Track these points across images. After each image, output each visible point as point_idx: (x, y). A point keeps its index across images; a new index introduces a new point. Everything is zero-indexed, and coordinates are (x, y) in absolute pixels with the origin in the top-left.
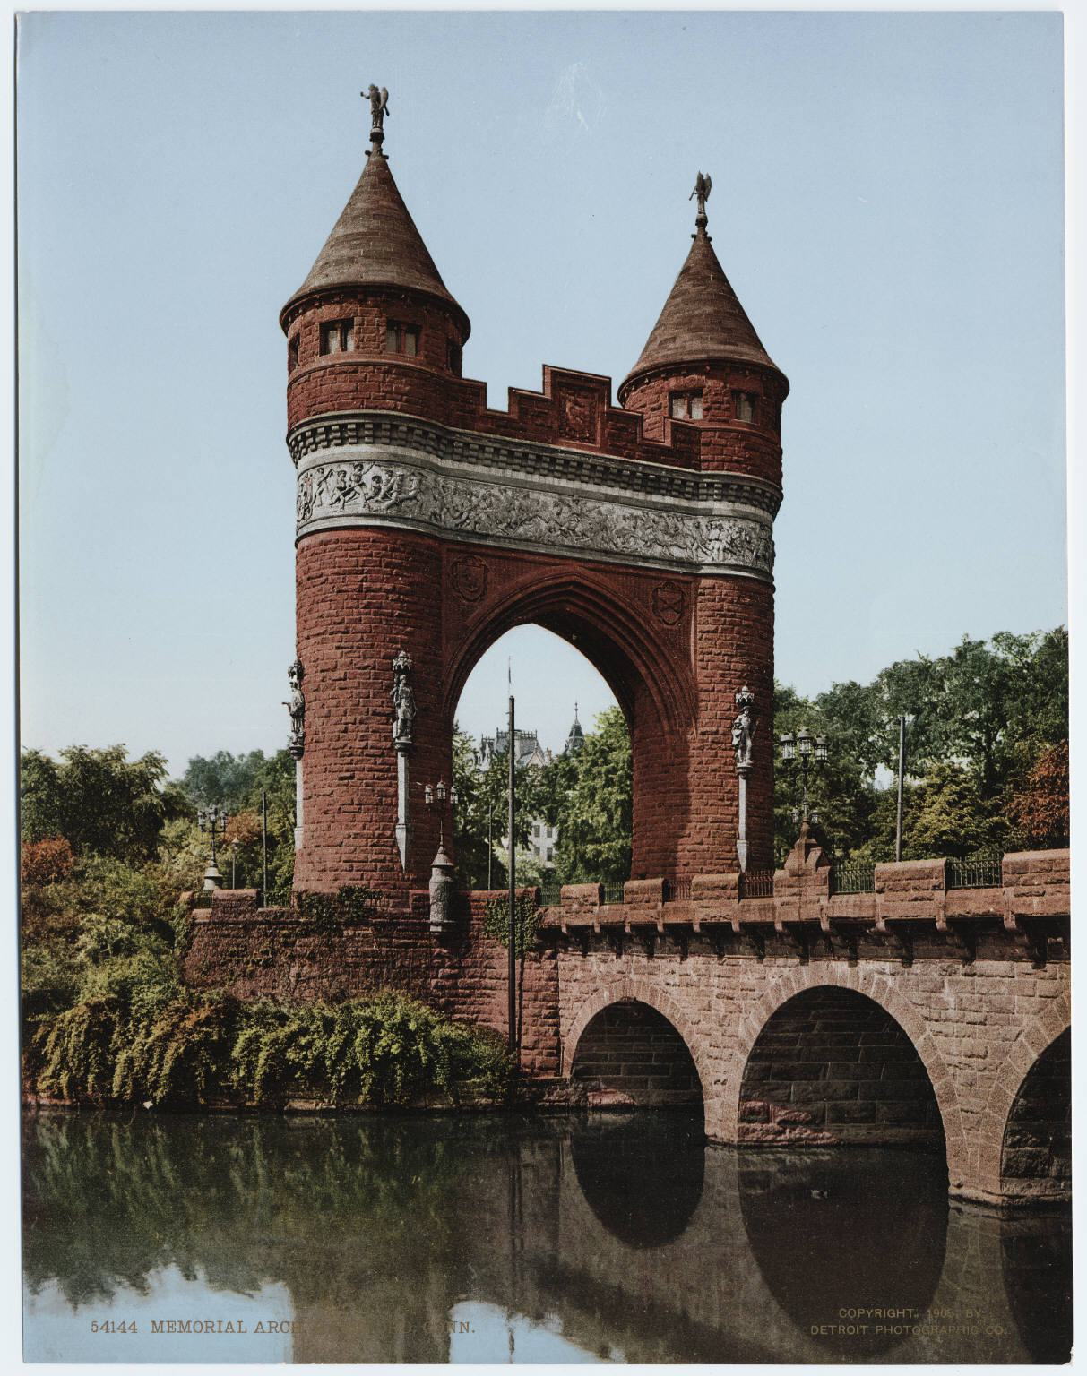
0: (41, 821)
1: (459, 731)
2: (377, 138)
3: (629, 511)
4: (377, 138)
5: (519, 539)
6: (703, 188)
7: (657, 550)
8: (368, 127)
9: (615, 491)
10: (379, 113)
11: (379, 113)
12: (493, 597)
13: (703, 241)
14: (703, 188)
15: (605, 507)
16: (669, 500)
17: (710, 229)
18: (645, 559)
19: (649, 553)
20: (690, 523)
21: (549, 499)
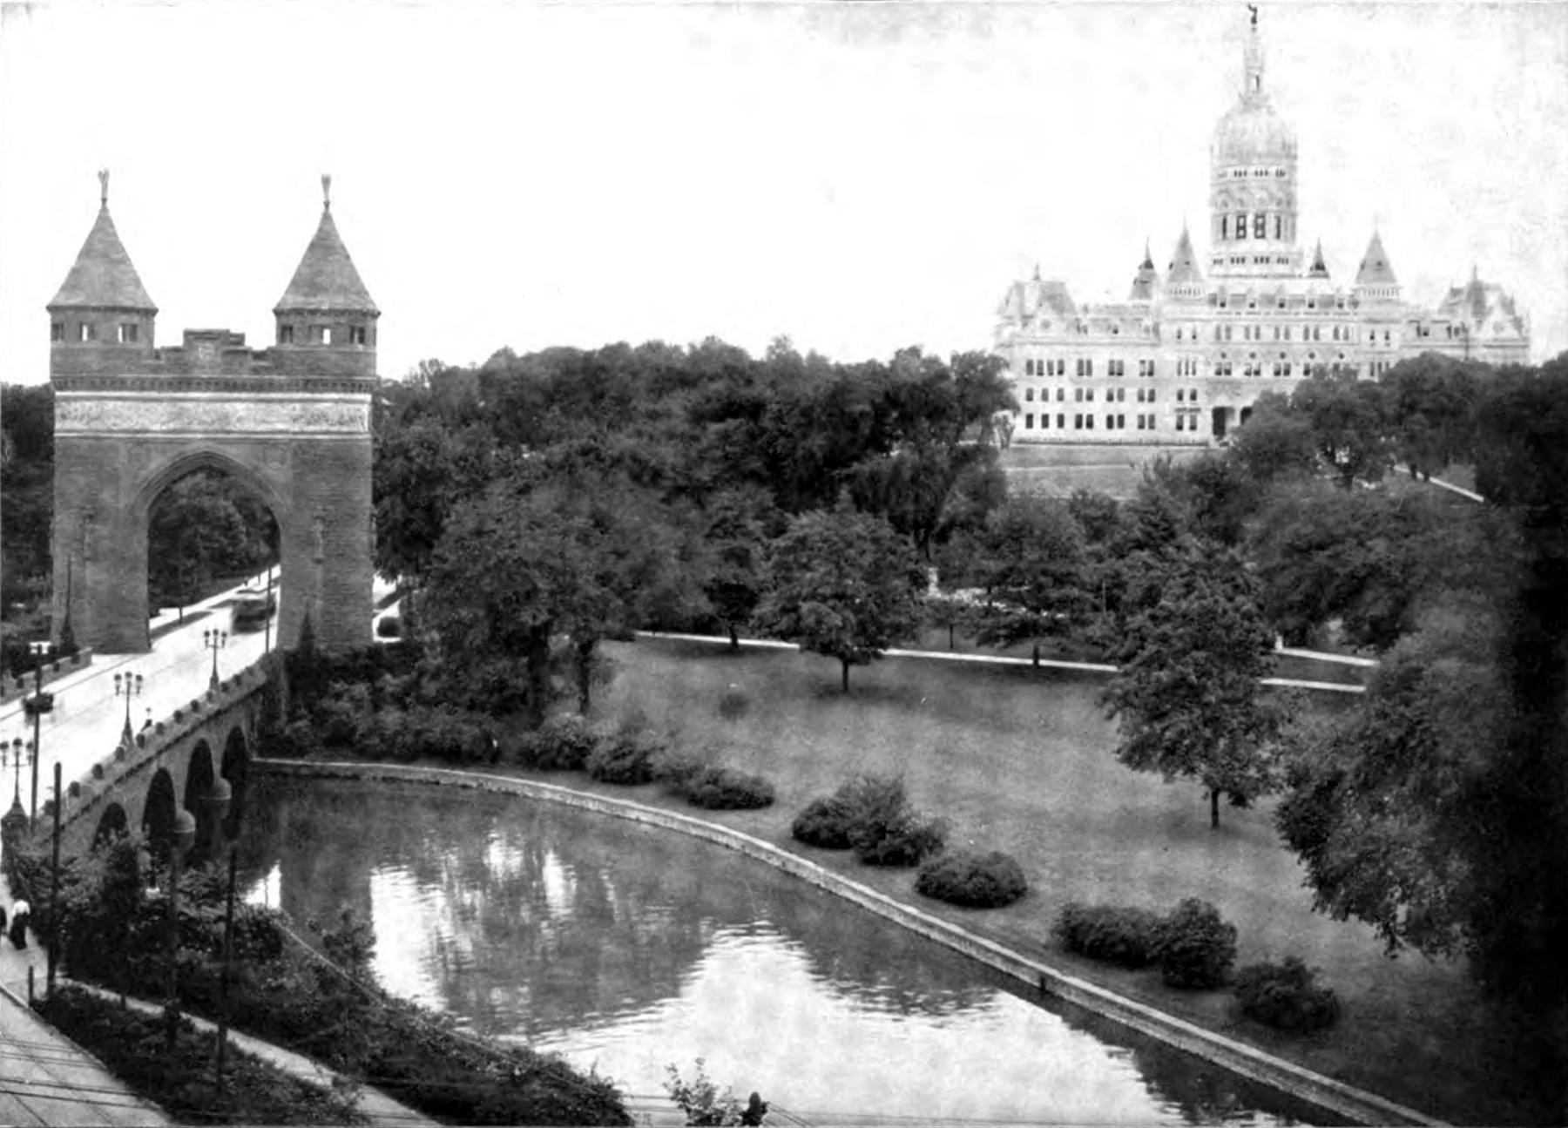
6: (326, 182)
13: (327, 217)
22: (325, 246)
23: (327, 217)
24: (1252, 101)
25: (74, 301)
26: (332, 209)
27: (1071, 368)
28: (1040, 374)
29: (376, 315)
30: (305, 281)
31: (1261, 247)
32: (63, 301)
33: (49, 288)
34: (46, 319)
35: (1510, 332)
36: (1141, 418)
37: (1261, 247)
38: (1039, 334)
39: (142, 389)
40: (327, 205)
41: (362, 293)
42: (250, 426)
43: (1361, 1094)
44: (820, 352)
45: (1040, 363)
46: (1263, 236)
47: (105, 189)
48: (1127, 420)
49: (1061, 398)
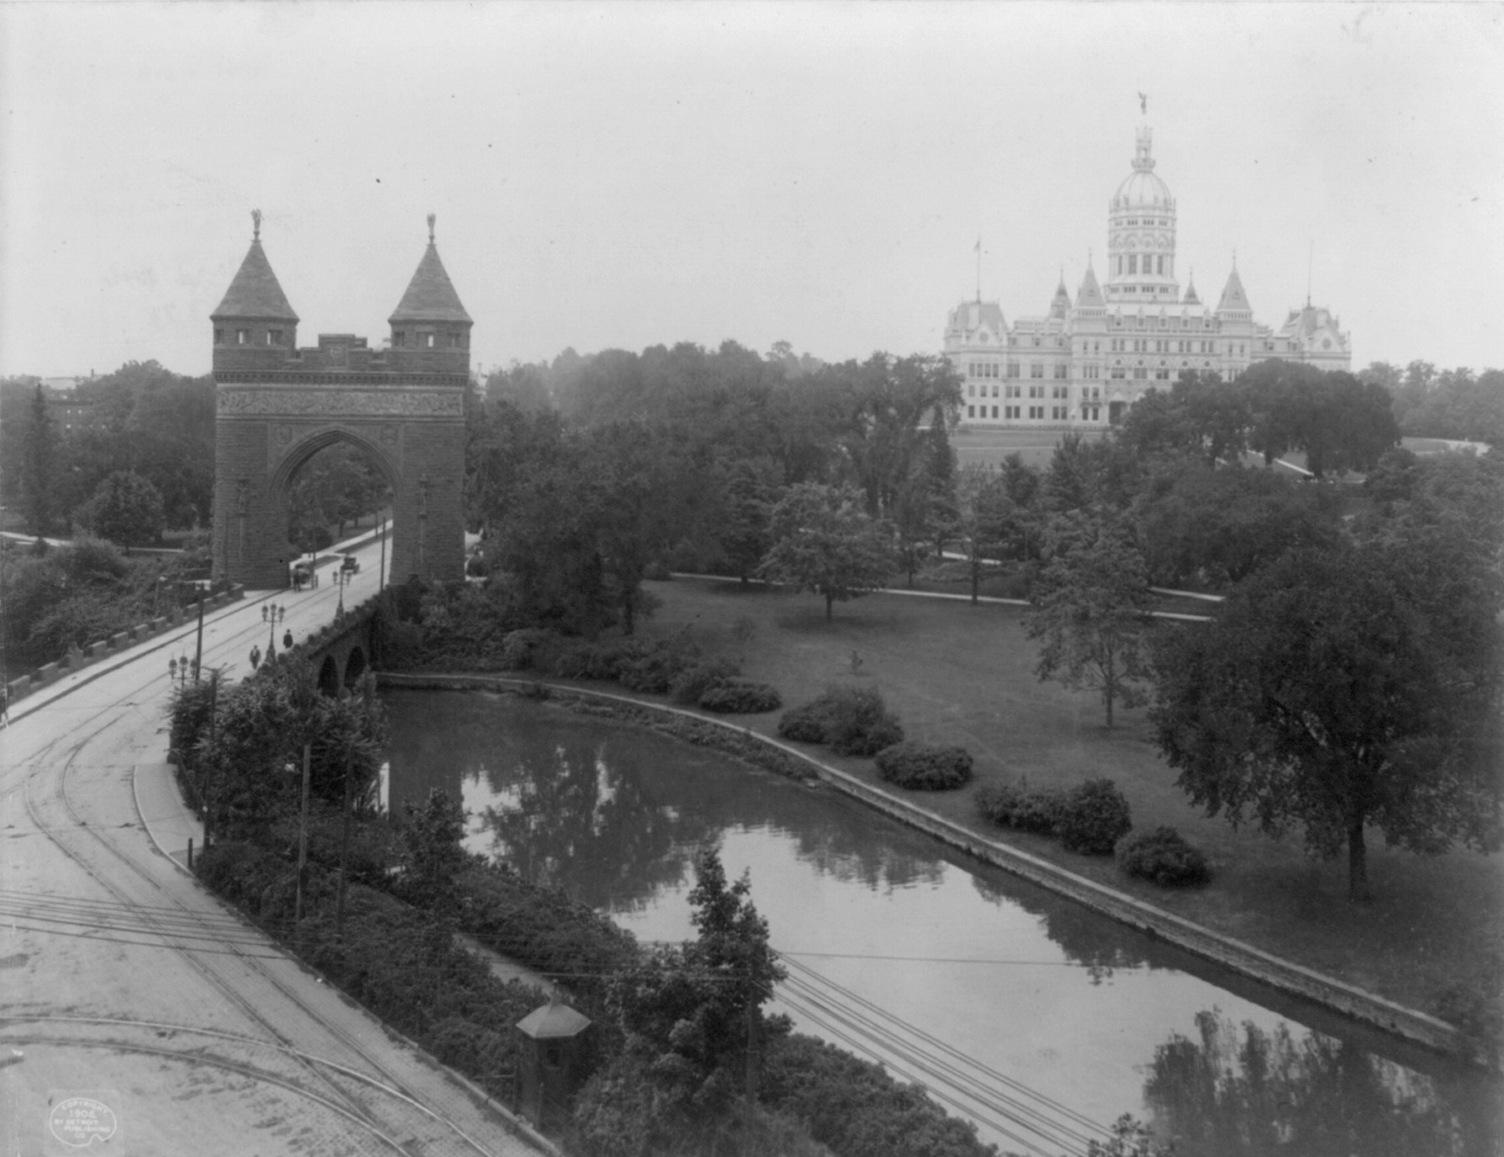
0: (310, 822)
1: (1263, 832)
2: (257, 233)
3: (367, 394)
4: (257, 233)
5: (306, 415)
6: (431, 220)
7: (381, 412)
8: (261, 228)
9: (359, 386)
10: (257, 223)
11: (257, 223)
12: (295, 441)
13: (432, 247)
14: (431, 220)
15: (352, 394)
16: (388, 387)
17: (435, 241)
18: (375, 416)
19: (377, 413)
20: (401, 396)
21: (324, 394)
22: (256, 263)
23: (432, 247)
27: (1003, 371)
37: (1147, 280)
49: (995, 395)
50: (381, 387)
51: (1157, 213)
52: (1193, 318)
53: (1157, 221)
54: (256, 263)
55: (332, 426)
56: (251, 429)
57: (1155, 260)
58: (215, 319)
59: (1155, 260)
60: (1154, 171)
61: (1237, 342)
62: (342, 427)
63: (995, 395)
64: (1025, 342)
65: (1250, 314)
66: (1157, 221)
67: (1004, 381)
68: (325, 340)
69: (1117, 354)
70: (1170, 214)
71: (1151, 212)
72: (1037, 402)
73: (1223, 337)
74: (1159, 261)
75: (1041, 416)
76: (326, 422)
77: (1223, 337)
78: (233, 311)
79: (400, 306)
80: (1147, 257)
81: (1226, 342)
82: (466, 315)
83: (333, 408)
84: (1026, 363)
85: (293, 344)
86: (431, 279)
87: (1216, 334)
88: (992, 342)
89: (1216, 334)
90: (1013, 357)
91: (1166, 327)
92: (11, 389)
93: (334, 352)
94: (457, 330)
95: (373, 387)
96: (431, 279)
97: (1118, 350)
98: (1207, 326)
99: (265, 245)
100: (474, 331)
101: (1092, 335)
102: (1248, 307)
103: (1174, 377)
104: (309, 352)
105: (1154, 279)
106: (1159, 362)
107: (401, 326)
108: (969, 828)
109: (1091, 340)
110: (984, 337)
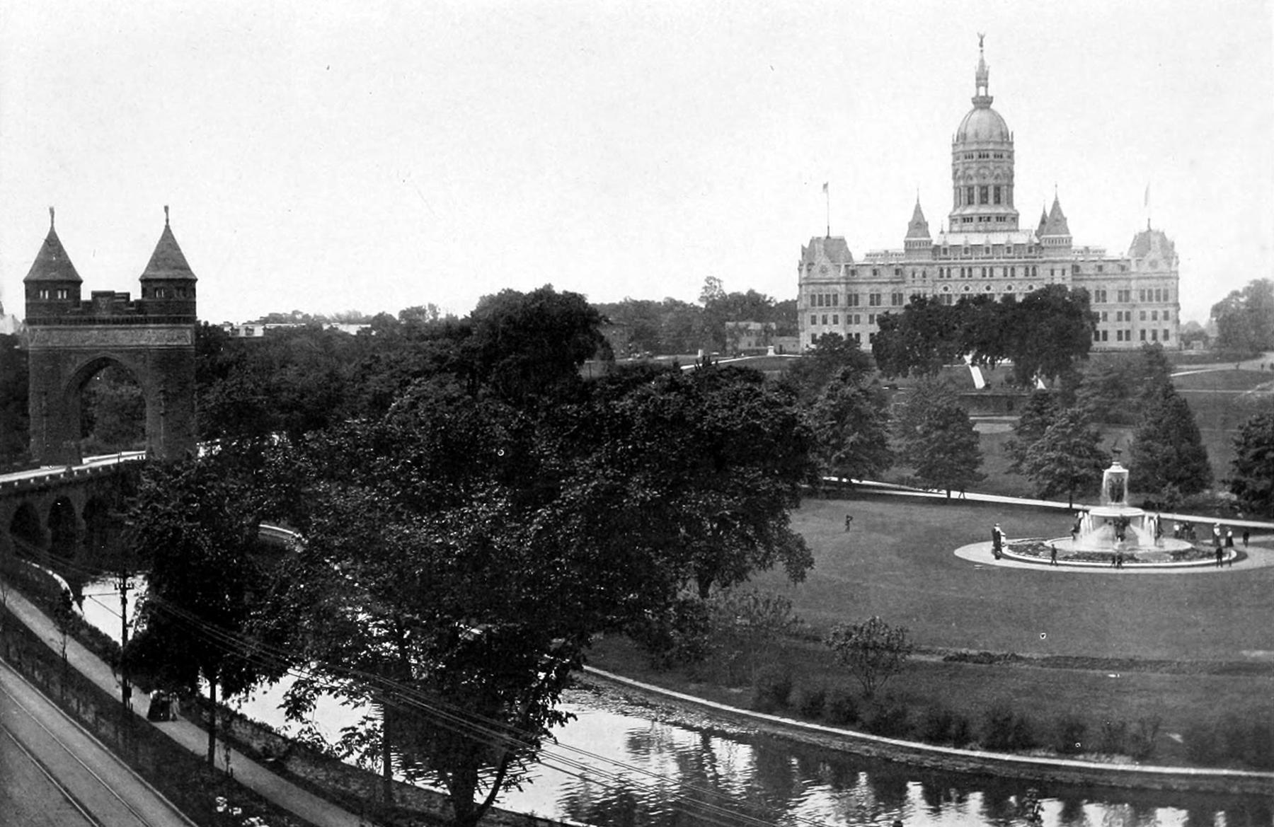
6: (166, 209)
13: (167, 227)
14: (166, 209)
22: (52, 243)
23: (167, 227)
24: (983, 103)
25: (162, 274)
26: (170, 223)
27: (842, 300)
28: (821, 304)
29: (196, 280)
30: (41, 263)
31: (984, 210)
32: (152, 275)
33: (25, 269)
34: (23, 286)
35: (1163, 267)
36: (1120, 332)
37: (984, 210)
38: (1150, 270)
39: (159, 323)
40: (167, 221)
41: (187, 268)
42: (125, 343)
43: (183, 815)
44: (759, 291)
45: (1158, 291)
46: (986, 202)
47: (53, 217)
48: (1110, 334)
49: (1155, 318)
50: (133, 326)
51: (991, 146)
52: (1016, 245)
53: (991, 154)
54: (52, 243)
55: (99, 355)
56: (55, 357)
57: (991, 192)
58: (27, 282)
59: (991, 192)
60: (992, 106)
61: (920, 269)
62: (108, 354)
63: (836, 322)
64: (887, 275)
65: (1070, 239)
66: (991, 154)
67: (845, 310)
68: (96, 295)
69: (1008, 280)
70: (1005, 147)
71: (984, 147)
72: (1124, 326)
73: (1044, 262)
74: (1000, 191)
75: (1128, 338)
76: (97, 351)
77: (1044, 262)
78: (36, 277)
79: (147, 268)
80: (984, 188)
81: (1049, 266)
82: (192, 274)
83: (103, 341)
84: (865, 291)
85: (79, 297)
86: (168, 249)
87: (1038, 259)
88: (831, 274)
89: (1038, 259)
90: (853, 287)
91: (1011, 255)
92: (1, 335)
93: (102, 302)
94: (187, 285)
95: (128, 326)
96: (168, 249)
97: (966, 277)
98: (1030, 251)
99: (56, 231)
100: (198, 285)
101: (921, 264)
102: (1067, 232)
103: (907, 302)
104: (87, 303)
105: (1001, 210)
106: (1027, 287)
107: (147, 283)
108: (1245, 770)
109: (920, 269)
110: (824, 270)
